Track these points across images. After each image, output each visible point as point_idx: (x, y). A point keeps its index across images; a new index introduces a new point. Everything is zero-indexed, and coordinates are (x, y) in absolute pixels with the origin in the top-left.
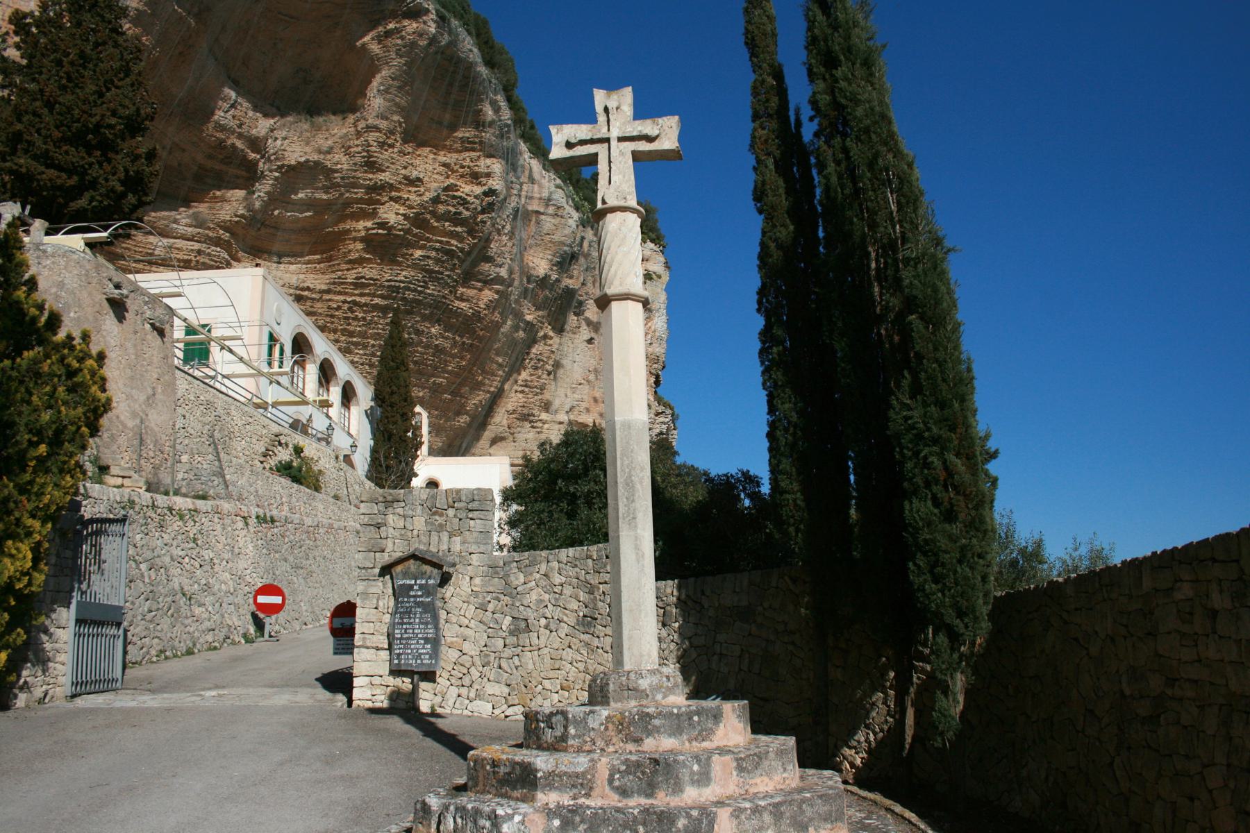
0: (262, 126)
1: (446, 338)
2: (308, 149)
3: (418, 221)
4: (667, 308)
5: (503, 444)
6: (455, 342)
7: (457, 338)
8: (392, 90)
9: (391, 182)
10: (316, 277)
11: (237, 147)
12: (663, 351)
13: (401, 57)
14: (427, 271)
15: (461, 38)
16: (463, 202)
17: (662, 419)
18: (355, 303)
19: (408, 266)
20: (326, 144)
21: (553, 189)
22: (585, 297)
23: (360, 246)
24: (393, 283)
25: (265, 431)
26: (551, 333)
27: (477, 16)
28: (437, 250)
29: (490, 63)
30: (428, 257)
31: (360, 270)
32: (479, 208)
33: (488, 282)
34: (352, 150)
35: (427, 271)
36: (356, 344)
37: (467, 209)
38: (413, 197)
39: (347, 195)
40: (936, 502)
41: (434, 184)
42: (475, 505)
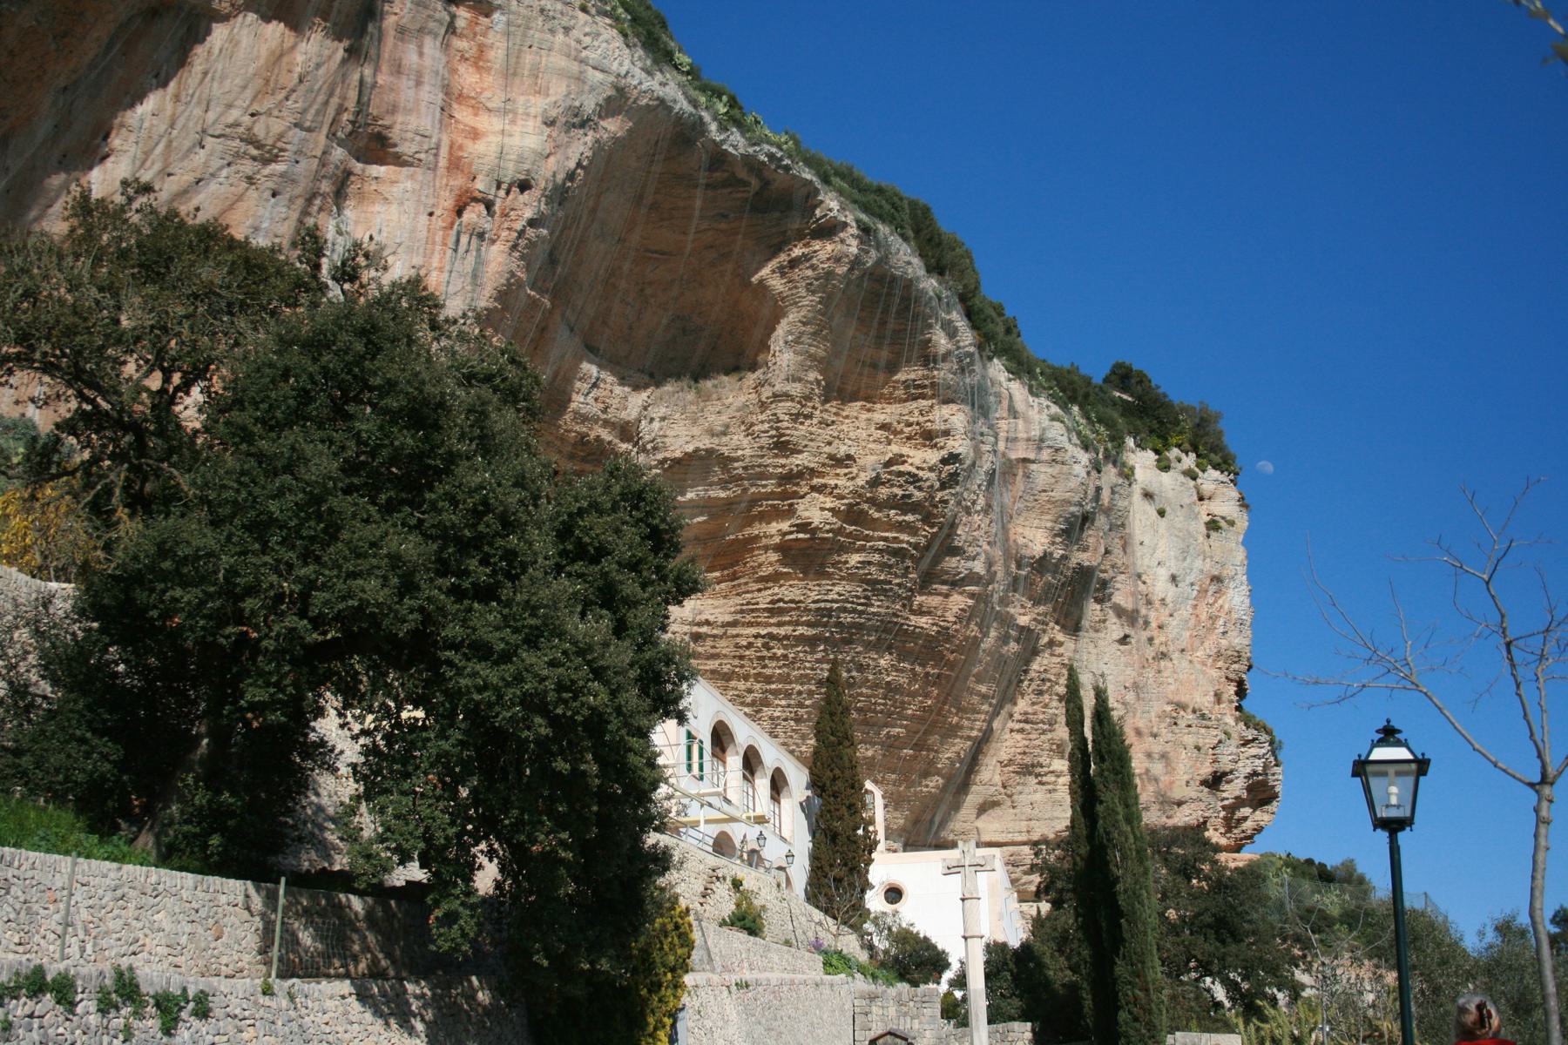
0: (632, 403)
1: (902, 671)
2: (696, 431)
3: (852, 515)
4: (1249, 574)
5: (997, 811)
6: (915, 674)
7: (918, 669)
8: (804, 339)
9: (812, 465)
10: (716, 603)
11: (603, 440)
12: (1246, 642)
13: (814, 293)
14: (867, 582)
15: (893, 250)
16: (914, 479)
17: (1254, 751)
18: (771, 636)
19: (842, 578)
20: (718, 422)
21: (1047, 423)
22: (1111, 573)
23: (773, 557)
24: (822, 605)
25: (702, 867)
26: (1060, 637)
27: (914, 205)
28: (880, 551)
29: (936, 268)
30: (869, 563)
31: (776, 590)
32: (937, 485)
33: (956, 583)
34: (756, 428)
35: (867, 582)
36: (775, 693)
37: (920, 489)
38: (841, 482)
39: (753, 490)
40: (1130, 1012)
41: (870, 461)
42: (926, 999)
